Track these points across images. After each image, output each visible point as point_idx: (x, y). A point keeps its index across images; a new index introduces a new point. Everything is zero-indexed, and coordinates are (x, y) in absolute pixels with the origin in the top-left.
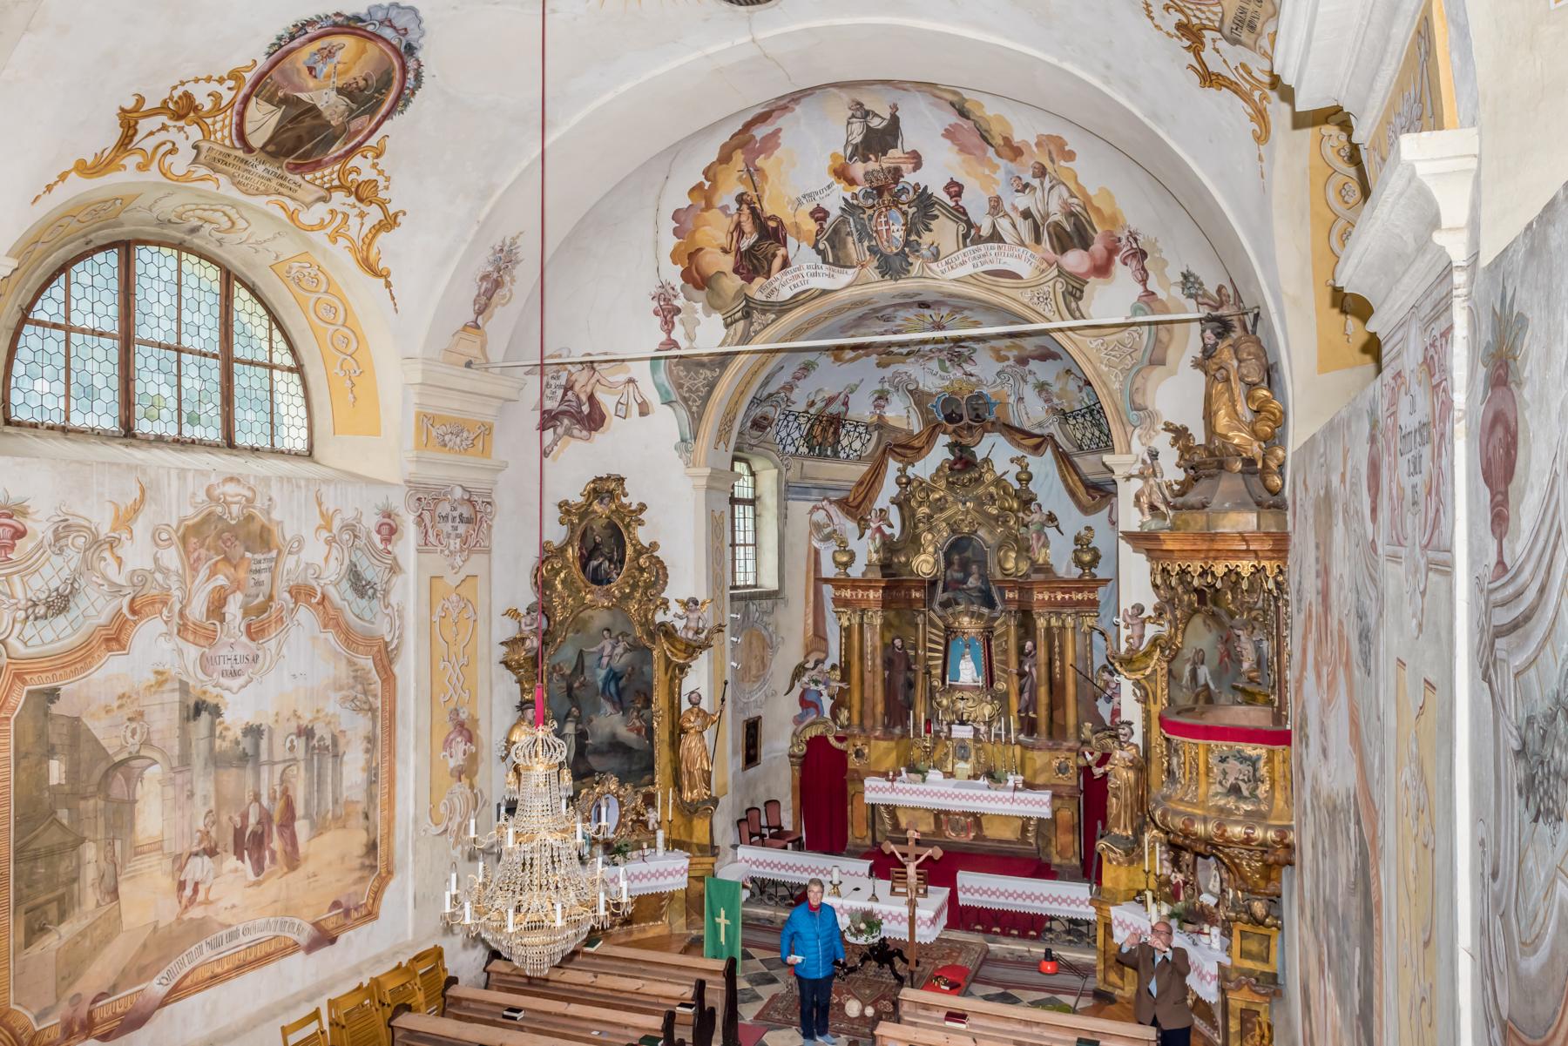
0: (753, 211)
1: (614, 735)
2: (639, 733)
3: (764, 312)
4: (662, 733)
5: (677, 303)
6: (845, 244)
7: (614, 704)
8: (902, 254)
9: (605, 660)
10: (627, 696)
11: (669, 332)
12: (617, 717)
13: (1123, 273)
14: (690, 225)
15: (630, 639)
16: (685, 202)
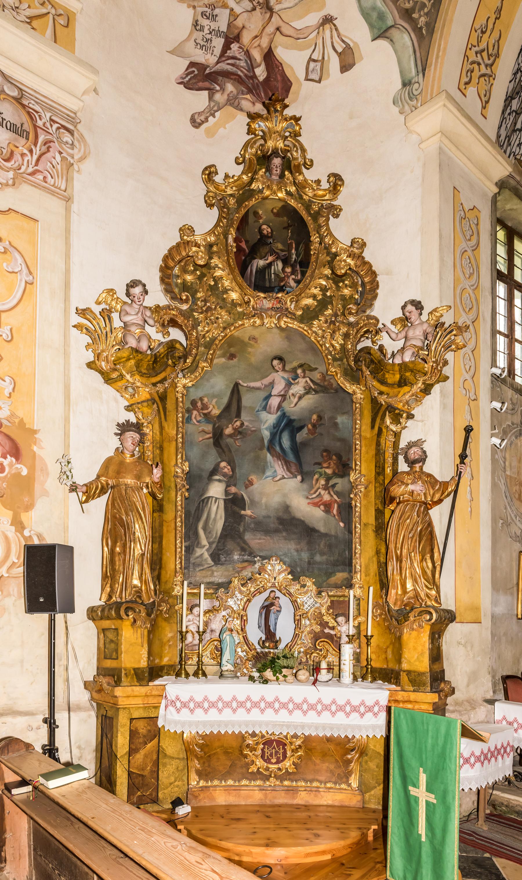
1: (287, 508)
2: (328, 507)
4: (364, 509)
7: (287, 463)
9: (275, 402)
10: (308, 457)
12: (293, 483)
15: (317, 376)
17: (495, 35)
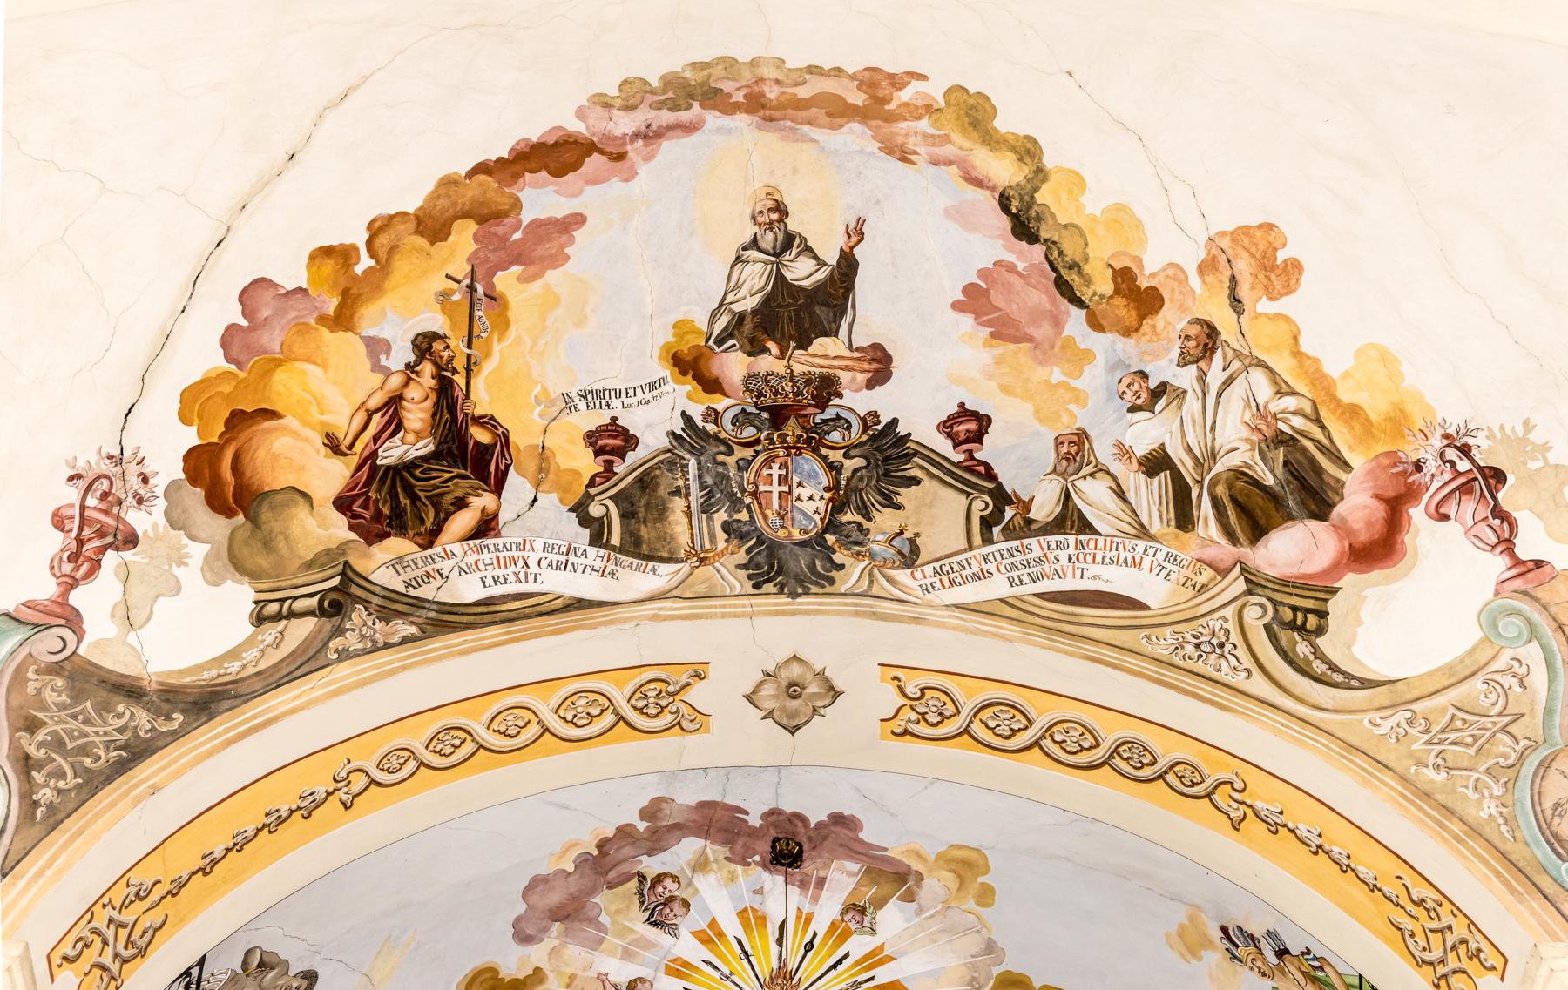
0: (444, 387)
3: (386, 615)
5: (136, 519)
6: (662, 512)
8: (816, 544)
11: (71, 584)
13: (1444, 549)
14: (273, 339)
16: (292, 274)
17: (155, 918)
